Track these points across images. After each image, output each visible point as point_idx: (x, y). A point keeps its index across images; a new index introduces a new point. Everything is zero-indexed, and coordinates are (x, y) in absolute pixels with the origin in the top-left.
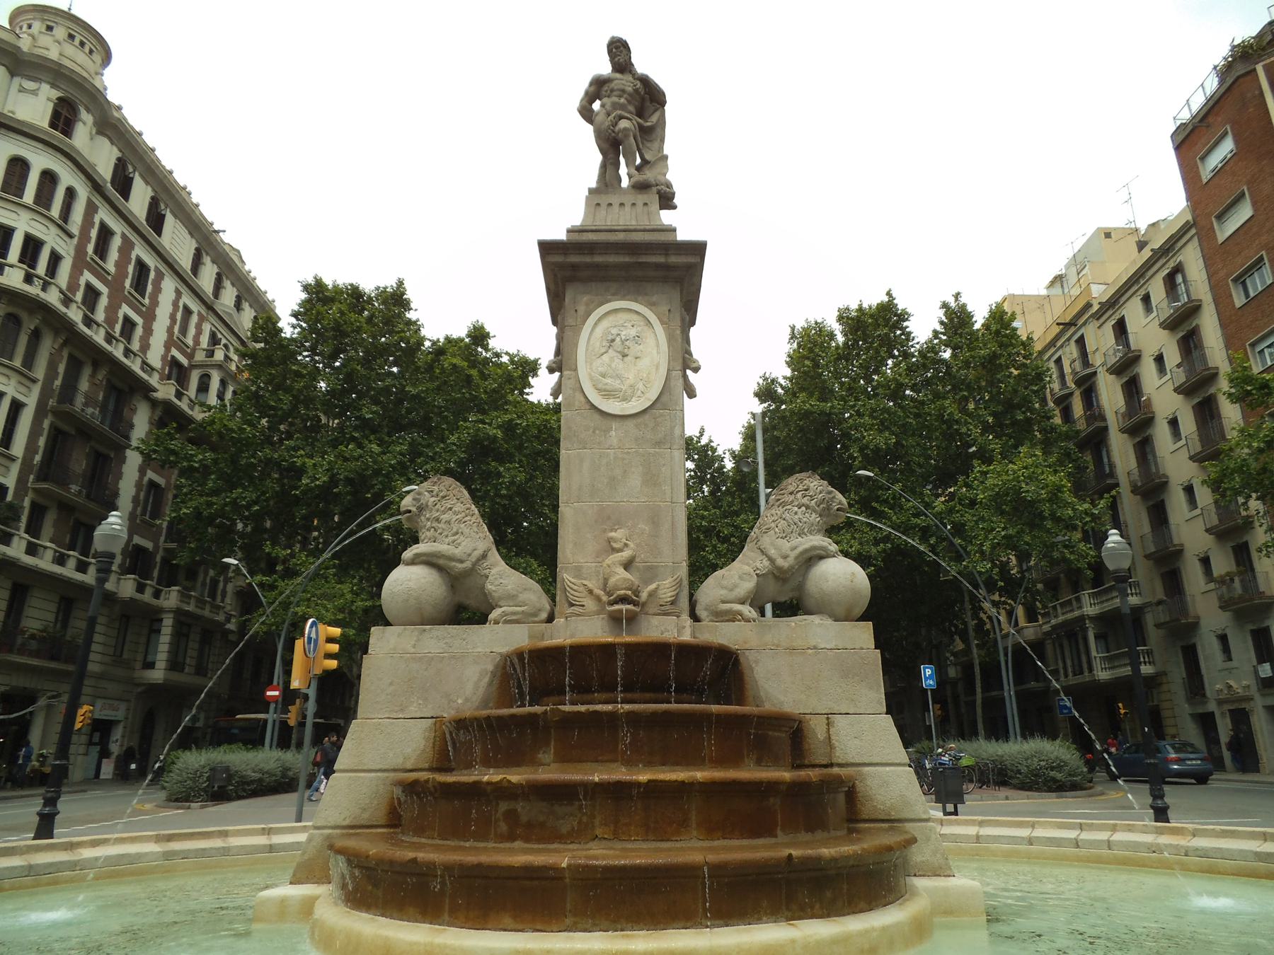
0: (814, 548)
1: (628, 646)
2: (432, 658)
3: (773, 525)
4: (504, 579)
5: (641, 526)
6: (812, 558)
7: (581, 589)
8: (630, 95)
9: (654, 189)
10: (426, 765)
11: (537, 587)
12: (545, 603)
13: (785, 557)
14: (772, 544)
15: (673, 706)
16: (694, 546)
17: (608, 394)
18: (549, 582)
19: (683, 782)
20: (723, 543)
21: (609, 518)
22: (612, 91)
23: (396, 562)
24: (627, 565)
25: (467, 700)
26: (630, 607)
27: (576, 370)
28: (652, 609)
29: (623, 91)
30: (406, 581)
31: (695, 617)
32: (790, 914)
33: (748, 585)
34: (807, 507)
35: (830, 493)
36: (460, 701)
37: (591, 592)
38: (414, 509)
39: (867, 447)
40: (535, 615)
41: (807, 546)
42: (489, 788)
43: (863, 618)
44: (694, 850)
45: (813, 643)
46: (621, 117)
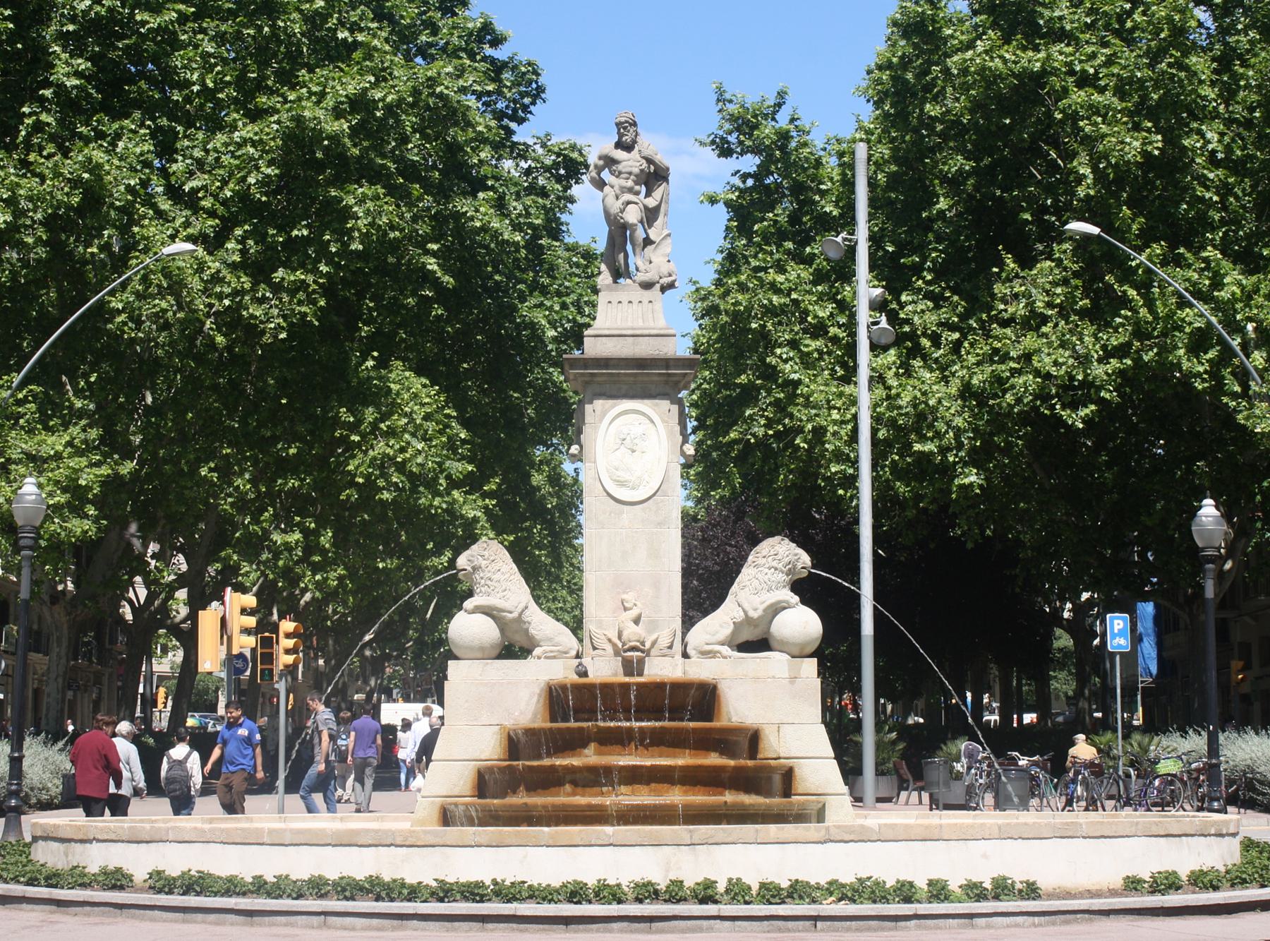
1: (639, 685)
4: (542, 624)
6: (776, 610)
9: (658, 286)
13: (755, 610)
15: (666, 724)
16: (683, 622)
17: (621, 484)
18: (576, 627)
20: (814, 337)
22: (620, 173)
24: (637, 621)
26: (639, 654)
28: (653, 652)
29: (630, 173)
30: (466, 627)
31: (685, 655)
33: (728, 630)
37: (610, 640)
38: (469, 568)
39: (1105, 156)
40: (566, 653)
41: (773, 601)
44: (676, 797)
46: (629, 203)
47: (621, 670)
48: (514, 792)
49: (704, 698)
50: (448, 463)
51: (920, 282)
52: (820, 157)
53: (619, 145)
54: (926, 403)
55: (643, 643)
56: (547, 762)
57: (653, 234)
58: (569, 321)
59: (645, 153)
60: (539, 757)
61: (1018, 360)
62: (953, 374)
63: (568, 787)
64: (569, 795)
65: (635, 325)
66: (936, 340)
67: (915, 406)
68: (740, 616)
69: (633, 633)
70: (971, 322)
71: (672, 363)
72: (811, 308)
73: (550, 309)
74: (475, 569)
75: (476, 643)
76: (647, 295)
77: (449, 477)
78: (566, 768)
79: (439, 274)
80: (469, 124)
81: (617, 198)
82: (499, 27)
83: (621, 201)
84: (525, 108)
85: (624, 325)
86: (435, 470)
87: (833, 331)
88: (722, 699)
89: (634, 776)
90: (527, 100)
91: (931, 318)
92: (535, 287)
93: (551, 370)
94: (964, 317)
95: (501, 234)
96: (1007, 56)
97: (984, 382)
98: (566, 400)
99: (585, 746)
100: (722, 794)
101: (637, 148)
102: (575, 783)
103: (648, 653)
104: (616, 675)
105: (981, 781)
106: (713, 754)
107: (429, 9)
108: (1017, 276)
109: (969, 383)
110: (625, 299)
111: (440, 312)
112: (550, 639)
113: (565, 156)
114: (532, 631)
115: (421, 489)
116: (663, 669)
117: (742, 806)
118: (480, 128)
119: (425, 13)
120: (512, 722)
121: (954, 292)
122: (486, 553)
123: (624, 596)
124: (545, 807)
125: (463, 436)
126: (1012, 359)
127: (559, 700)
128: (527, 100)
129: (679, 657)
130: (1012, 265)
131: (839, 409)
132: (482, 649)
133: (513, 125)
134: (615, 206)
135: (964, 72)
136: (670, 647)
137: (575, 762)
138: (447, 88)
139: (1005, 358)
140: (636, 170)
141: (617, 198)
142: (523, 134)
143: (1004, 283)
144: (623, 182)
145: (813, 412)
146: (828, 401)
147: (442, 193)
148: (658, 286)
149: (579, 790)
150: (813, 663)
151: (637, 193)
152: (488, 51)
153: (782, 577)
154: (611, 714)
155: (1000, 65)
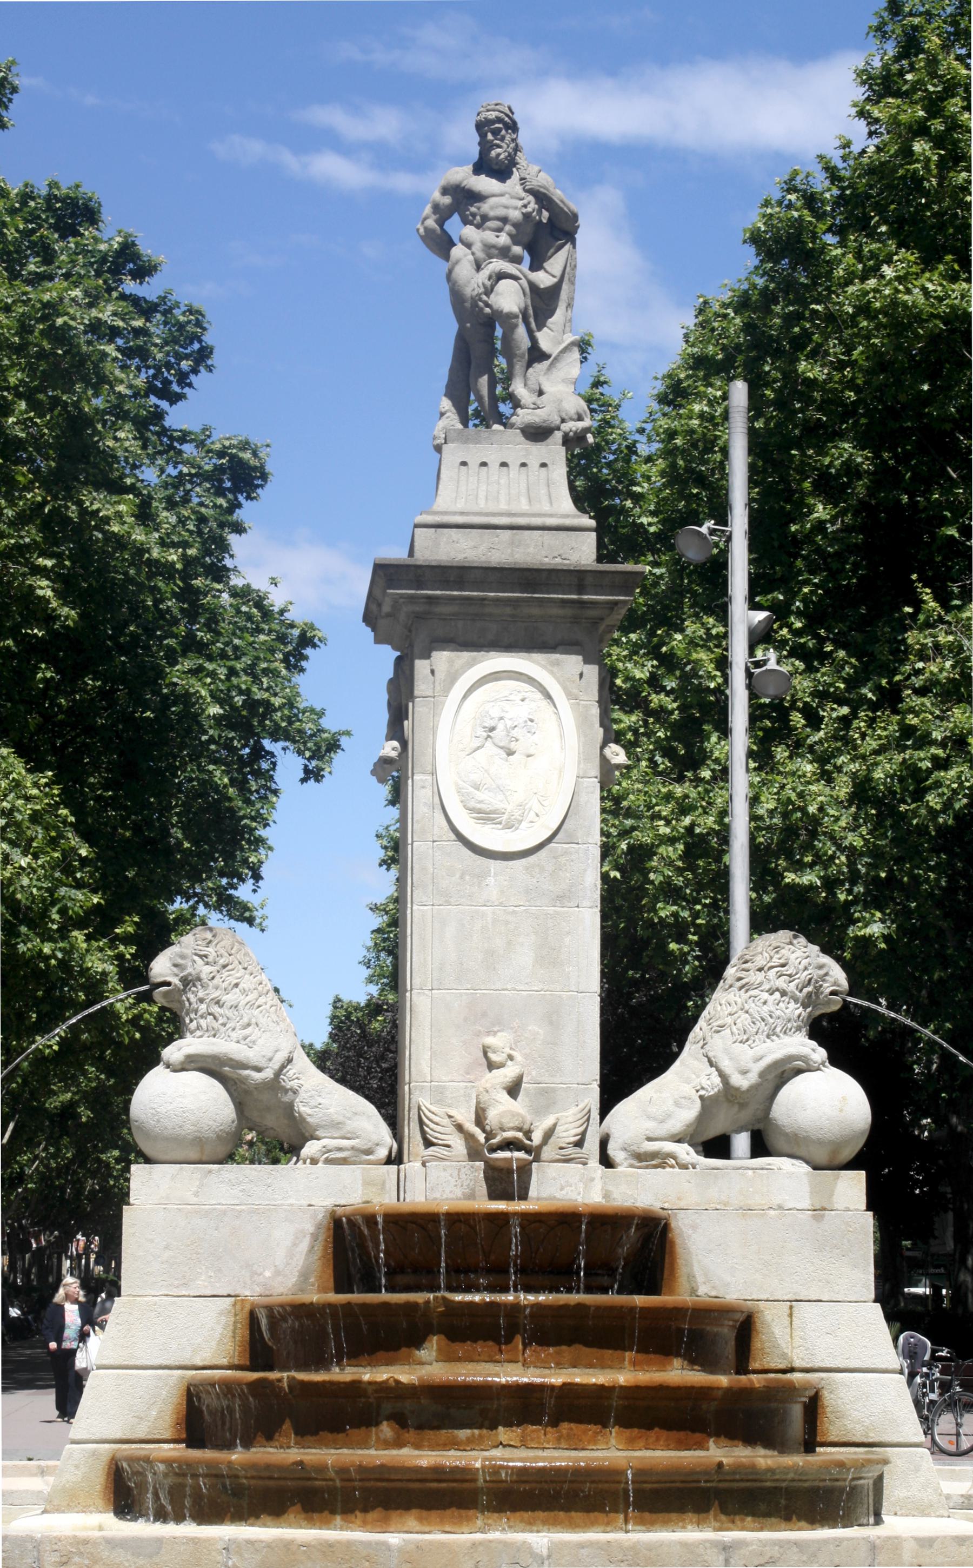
0: (790, 1058)
1: (529, 1219)
2: (224, 1213)
3: (729, 1020)
5: (533, 1027)
6: (783, 1073)
7: (446, 1121)
8: (515, 225)
9: (558, 435)
10: (225, 1362)
11: (371, 1109)
12: (383, 1132)
13: (744, 1072)
14: (726, 1051)
15: (384, 1296)
17: (485, 816)
19: (602, 1386)
21: (484, 1015)
22: (485, 218)
23: (153, 1060)
24: (513, 1090)
25: (277, 1273)
27: (434, 773)
28: (547, 1153)
29: (505, 220)
30: (169, 1097)
31: (606, 1161)
32: (717, 1525)
33: (689, 1114)
34: (784, 993)
35: (820, 967)
36: (268, 1274)
37: (460, 1128)
38: (175, 981)
40: (369, 1152)
42: (370, 1389)
43: (851, 1165)
44: (611, 1451)
45: (776, 1201)
46: (501, 276)
47: (482, 1189)
48: (269, 1437)
49: (644, 1246)
50: (63, 891)
51: (785, 631)
52: (635, 442)
53: (483, 166)
54: (803, 810)
55: (528, 1134)
56: (342, 1374)
57: (545, 340)
58: (241, 692)
59: (534, 183)
60: (321, 1363)
61: (943, 744)
62: (839, 769)
63: (386, 1430)
64: (387, 1445)
65: (514, 508)
66: (814, 721)
67: (786, 815)
68: (713, 1084)
69: (503, 1110)
70: (864, 691)
71: (589, 580)
72: (620, 665)
73: (213, 674)
74: (187, 982)
75: (189, 1129)
76: (537, 452)
77: (63, 912)
78: (382, 1388)
79: (54, 604)
80: (103, 379)
81: (478, 267)
82: (146, 249)
83: (486, 272)
84: (183, 379)
85: (492, 507)
86: (44, 900)
87: (656, 700)
88: (679, 1250)
89: (525, 1407)
90: (185, 365)
91: (803, 684)
92: (191, 645)
93: (211, 767)
94: (853, 683)
95: (148, 551)
96: (931, 287)
97: (892, 777)
98: (232, 810)
99: (417, 1341)
100: (702, 1446)
101: (516, 175)
102: (400, 1421)
103: (536, 1153)
104: (471, 1196)
105: (933, 1396)
106: (677, 1362)
107: (40, 227)
108: (941, 620)
109: (868, 779)
110: (494, 458)
111: (49, 675)
112: (337, 1125)
113: (233, 457)
114: (301, 1108)
115: (23, 929)
116: (563, 1186)
117: (750, 1473)
118: (121, 388)
119: (33, 231)
120: (258, 1290)
121: (838, 644)
122: (211, 950)
123: (489, 1040)
124: (343, 1471)
125: (83, 852)
126: (933, 743)
127: (351, 1244)
128: (185, 365)
129: (594, 1162)
130: (932, 604)
131: (665, 819)
132: (199, 1141)
133: (164, 404)
134: (472, 281)
135: (864, 310)
136: (579, 1144)
137: (405, 1375)
138: (73, 319)
139: (924, 741)
140: (515, 215)
141: (478, 267)
142: (178, 417)
143: (921, 629)
144: (490, 237)
145: (629, 822)
146: (649, 807)
147: (60, 483)
148: (558, 435)
149: (411, 1435)
150: (858, 1179)
151: (517, 260)
152: (130, 286)
153: (795, 1010)
154: (462, 1277)
155: (921, 299)
